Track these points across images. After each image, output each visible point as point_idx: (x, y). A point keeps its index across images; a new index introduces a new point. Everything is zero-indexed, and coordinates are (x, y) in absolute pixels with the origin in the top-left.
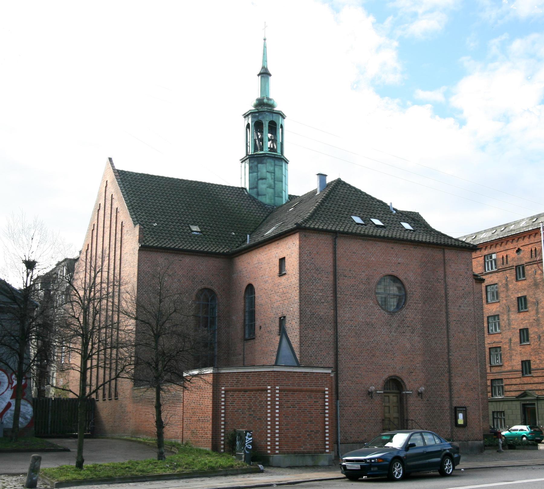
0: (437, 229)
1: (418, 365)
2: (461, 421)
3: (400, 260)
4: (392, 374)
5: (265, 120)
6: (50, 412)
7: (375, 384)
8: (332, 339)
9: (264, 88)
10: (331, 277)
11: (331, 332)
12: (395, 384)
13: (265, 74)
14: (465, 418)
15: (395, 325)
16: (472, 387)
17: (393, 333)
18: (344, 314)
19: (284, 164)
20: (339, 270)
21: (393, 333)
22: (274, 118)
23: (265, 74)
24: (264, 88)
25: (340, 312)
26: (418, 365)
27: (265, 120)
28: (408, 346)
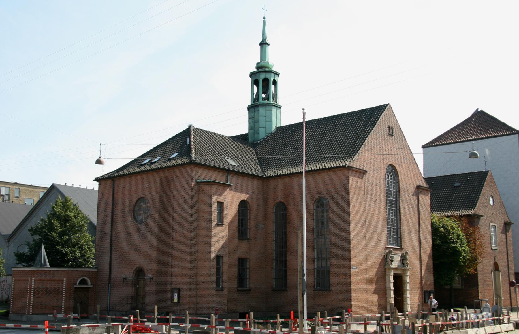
0: (469, 116)
1: (153, 258)
2: (176, 300)
3: (148, 185)
4: (138, 266)
5: (263, 79)
6: (199, 318)
7: (129, 272)
8: (109, 246)
9: (263, 54)
10: (111, 206)
11: (109, 241)
12: (140, 272)
13: (263, 44)
14: (179, 297)
15: (142, 232)
16: (186, 273)
17: (141, 238)
18: (117, 228)
19: (274, 110)
20: (116, 201)
21: (141, 238)
22: (268, 76)
23: (263, 44)
24: (263, 54)
25: (115, 227)
26: (153, 258)
27: (263, 79)
28: (148, 245)
